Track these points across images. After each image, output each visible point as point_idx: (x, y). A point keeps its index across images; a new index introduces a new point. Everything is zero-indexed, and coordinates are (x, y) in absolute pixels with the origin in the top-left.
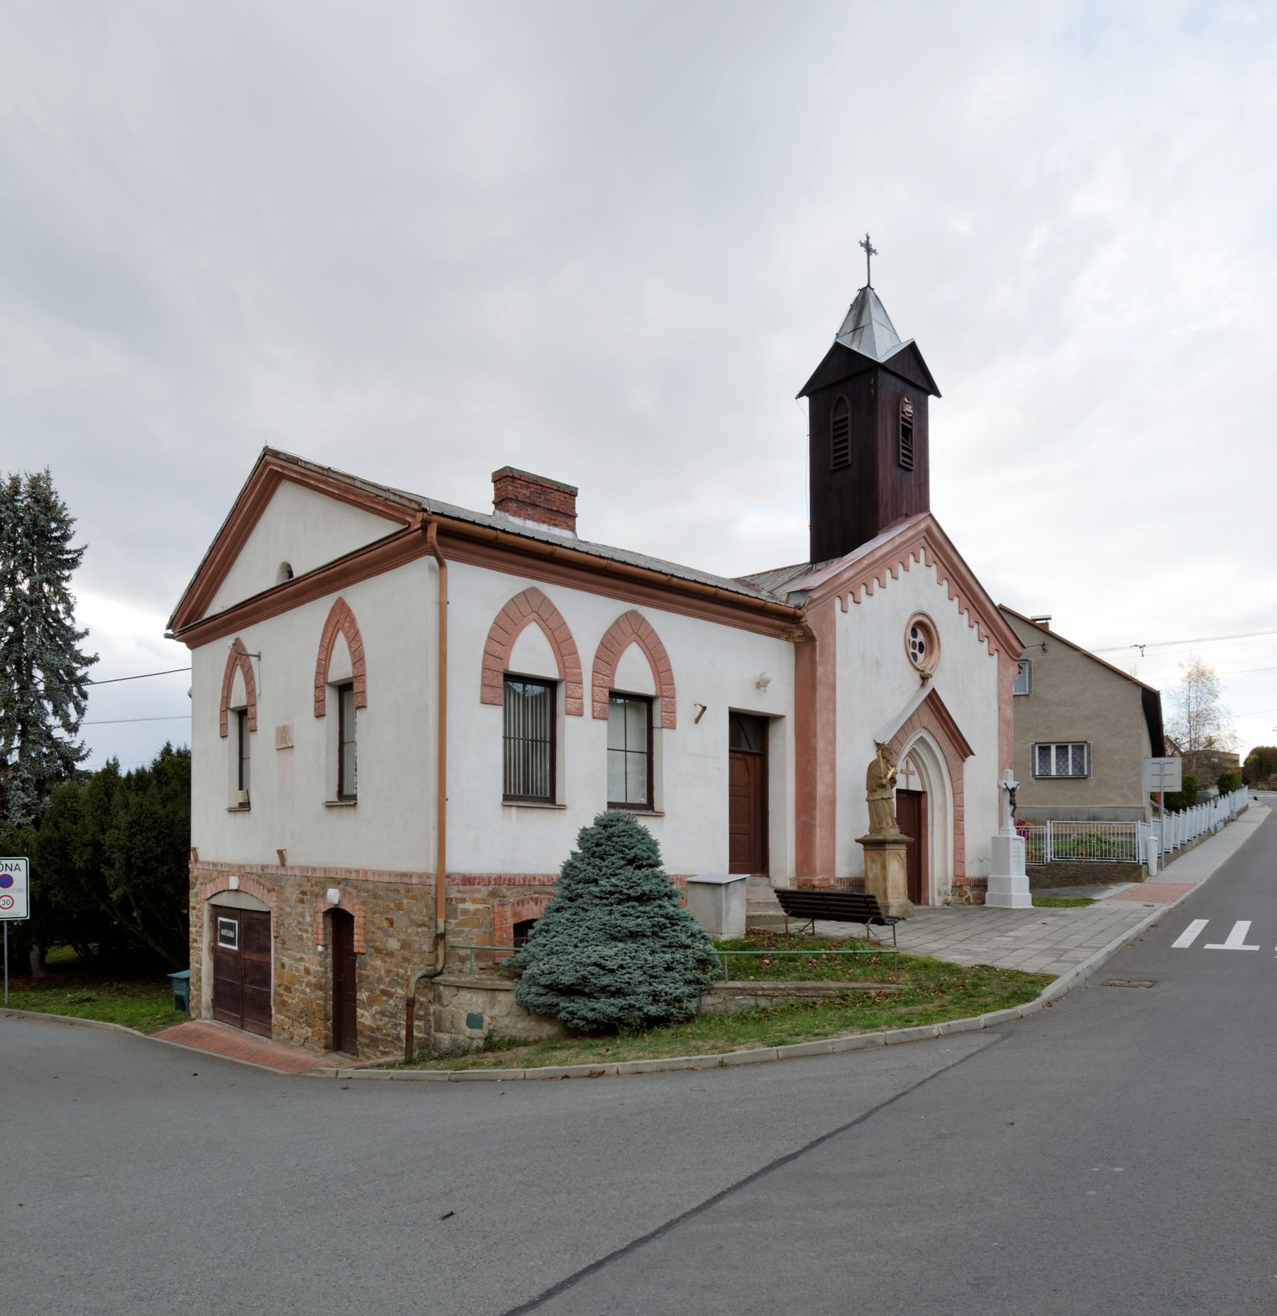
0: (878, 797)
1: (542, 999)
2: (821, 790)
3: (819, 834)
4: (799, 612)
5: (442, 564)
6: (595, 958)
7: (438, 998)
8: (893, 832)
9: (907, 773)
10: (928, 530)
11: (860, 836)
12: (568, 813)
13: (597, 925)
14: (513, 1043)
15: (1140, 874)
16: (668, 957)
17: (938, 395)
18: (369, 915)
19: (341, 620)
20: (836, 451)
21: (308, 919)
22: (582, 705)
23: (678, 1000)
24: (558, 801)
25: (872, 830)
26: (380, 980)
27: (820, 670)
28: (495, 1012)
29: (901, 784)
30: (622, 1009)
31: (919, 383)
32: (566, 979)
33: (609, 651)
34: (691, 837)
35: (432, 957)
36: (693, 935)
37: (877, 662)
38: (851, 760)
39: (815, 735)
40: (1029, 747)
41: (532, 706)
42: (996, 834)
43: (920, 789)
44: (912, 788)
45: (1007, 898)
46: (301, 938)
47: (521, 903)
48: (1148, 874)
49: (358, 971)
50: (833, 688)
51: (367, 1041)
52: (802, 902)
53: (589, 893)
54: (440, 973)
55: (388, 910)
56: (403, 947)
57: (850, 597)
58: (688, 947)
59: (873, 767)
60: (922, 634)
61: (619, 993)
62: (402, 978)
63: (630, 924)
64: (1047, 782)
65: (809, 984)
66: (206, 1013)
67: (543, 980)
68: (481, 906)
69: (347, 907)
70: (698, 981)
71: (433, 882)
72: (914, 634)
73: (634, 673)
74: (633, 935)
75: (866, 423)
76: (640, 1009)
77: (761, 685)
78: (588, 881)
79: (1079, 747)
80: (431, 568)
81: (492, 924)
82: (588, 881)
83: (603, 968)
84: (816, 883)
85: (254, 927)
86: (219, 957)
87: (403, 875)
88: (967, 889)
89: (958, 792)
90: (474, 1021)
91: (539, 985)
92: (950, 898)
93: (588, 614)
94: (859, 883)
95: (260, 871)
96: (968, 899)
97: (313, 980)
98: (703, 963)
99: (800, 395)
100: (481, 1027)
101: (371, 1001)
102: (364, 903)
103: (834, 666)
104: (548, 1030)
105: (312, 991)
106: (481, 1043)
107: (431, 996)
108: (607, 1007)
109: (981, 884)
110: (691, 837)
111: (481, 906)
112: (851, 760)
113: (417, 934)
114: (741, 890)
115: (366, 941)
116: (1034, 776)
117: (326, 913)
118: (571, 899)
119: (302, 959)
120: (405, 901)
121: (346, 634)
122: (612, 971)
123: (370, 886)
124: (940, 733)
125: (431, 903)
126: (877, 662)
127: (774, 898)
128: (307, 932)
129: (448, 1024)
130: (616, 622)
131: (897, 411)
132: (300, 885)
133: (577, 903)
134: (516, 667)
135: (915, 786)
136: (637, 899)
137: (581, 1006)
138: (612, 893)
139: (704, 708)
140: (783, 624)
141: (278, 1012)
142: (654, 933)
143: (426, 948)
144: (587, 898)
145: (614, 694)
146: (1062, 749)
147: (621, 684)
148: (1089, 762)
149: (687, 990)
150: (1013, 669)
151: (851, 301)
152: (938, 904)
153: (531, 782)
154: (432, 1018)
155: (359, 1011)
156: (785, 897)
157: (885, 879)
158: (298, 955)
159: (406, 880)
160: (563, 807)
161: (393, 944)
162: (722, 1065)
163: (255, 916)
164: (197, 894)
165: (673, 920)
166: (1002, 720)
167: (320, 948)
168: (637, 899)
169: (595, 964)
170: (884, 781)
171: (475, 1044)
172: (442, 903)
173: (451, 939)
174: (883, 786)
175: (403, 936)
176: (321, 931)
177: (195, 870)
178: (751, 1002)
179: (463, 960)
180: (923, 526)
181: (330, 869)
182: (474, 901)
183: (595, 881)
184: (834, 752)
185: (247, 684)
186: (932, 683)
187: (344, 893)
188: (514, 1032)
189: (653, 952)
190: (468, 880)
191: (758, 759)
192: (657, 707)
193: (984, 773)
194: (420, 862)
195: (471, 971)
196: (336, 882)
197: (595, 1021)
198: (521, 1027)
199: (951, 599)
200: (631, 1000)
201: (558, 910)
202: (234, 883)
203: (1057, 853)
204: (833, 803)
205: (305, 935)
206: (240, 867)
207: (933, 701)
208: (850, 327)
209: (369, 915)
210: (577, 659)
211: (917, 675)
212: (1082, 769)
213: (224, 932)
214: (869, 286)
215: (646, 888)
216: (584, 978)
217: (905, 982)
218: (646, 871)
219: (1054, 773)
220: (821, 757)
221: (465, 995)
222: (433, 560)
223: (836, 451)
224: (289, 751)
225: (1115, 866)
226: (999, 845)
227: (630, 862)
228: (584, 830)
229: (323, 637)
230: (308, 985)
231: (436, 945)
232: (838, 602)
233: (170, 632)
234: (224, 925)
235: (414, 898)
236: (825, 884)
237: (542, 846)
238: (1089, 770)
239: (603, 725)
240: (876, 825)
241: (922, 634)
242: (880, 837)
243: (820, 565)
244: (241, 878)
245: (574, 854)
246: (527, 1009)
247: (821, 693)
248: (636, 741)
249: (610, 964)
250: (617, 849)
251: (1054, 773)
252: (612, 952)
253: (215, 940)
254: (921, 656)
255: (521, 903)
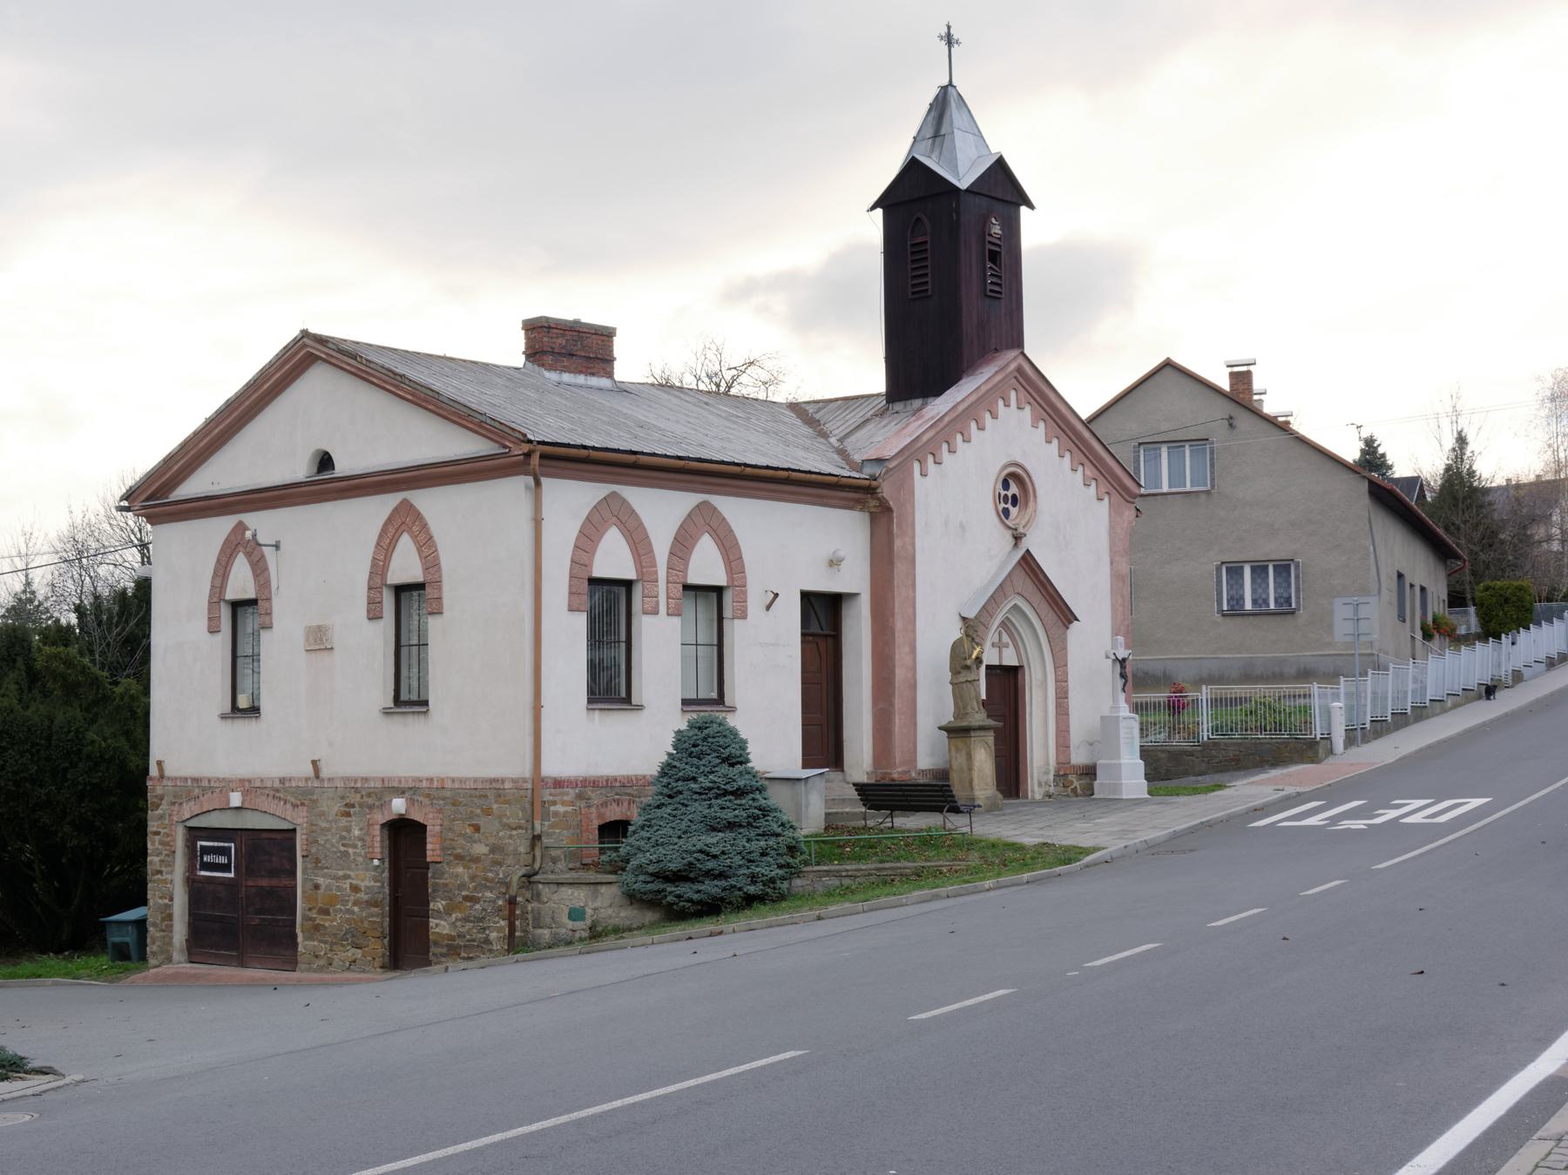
0: (962, 679)
1: (649, 886)
2: (900, 674)
3: (898, 721)
4: (874, 483)
5: (538, 483)
6: (700, 846)
7: (537, 897)
8: (979, 717)
9: (1000, 646)
10: (1019, 370)
11: (944, 723)
12: (645, 712)
13: (698, 818)
14: (617, 931)
15: (1317, 753)
16: (763, 843)
17: (1031, 206)
18: (446, 823)
19: (406, 521)
20: (915, 277)
21: (357, 833)
22: (657, 603)
23: (772, 881)
24: (634, 701)
25: (957, 716)
26: (462, 886)
27: (898, 543)
28: (598, 904)
29: (991, 657)
30: (724, 889)
31: (1009, 198)
32: (673, 866)
33: (682, 545)
34: (770, 733)
35: (530, 857)
36: (783, 825)
37: (962, 526)
38: (933, 635)
39: (893, 615)
40: (1212, 567)
41: (609, 607)
42: (1106, 713)
43: (1016, 663)
44: (1005, 663)
45: (1117, 787)
46: (346, 854)
47: (604, 805)
48: (1331, 752)
49: (431, 881)
50: (912, 561)
51: (444, 950)
52: (884, 795)
53: (690, 790)
54: (536, 873)
55: (472, 815)
56: (492, 851)
57: (930, 459)
58: (778, 835)
59: (956, 647)
60: (1015, 489)
61: (722, 875)
62: (492, 881)
63: (729, 815)
64: (1239, 620)
65: (887, 865)
66: (178, 956)
67: (651, 869)
68: (569, 809)
69: (417, 816)
70: (788, 866)
71: (529, 786)
72: (1006, 485)
73: (706, 566)
74: (731, 826)
75: (950, 261)
76: (740, 889)
77: (834, 563)
78: (686, 779)
79: (1283, 569)
80: (527, 488)
81: (580, 824)
82: (686, 779)
83: (708, 854)
84: (895, 776)
85: (268, 852)
86: (198, 893)
87: (496, 780)
88: (1072, 778)
89: (1061, 664)
90: (576, 914)
91: (647, 873)
92: (1052, 790)
93: (661, 511)
94: (943, 774)
95: (277, 784)
96: (1074, 791)
97: (363, 896)
98: (792, 849)
99: (873, 208)
100: (583, 919)
101: (449, 911)
102: (440, 811)
103: (913, 537)
104: (650, 916)
105: (362, 909)
106: (585, 934)
107: (529, 896)
108: (711, 888)
109: (1090, 772)
110: (770, 733)
111: (569, 809)
112: (933, 635)
113: (511, 837)
114: (820, 784)
115: (443, 849)
116: (1221, 611)
117: (383, 825)
118: (670, 797)
119: (347, 877)
120: (495, 806)
121: (414, 538)
122: (715, 857)
123: (448, 794)
124: (1037, 598)
125: (528, 806)
126: (962, 526)
127: (853, 794)
128: (355, 846)
129: (548, 920)
130: (689, 515)
131: (983, 233)
132: (343, 798)
133: (677, 799)
134: (598, 573)
135: (1010, 659)
136: (732, 793)
137: (686, 889)
138: (710, 789)
139: (776, 595)
140: (856, 496)
141: (308, 938)
142: (749, 824)
143: (522, 850)
144: (686, 794)
145: (687, 588)
146: (1259, 570)
147: (694, 578)
148: (1298, 589)
149: (780, 872)
150: (1129, 513)
151: (931, 99)
152: (1038, 797)
153: (610, 686)
154: (530, 916)
155: (433, 922)
156: (860, 788)
157: (970, 769)
158: (341, 873)
159: (498, 785)
160: (640, 708)
161: (480, 849)
162: (819, 918)
163: (265, 835)
164: (161, 817)
165: (765, 811)
166: (1116, 576)
167: (376, 862)
168: (732, 793)
169: (701, 851)
170: (968, 662)
171: (577, 935)
172: (538, 805)
173: (545, 840)
174: (968, 668)
175: (492, 840)
176: (377, 844)
177: (154, 788)
178: (837, 882)
179: (554, 861)
180: (1013, 366)
181: (390, 779)
182: (563, 803)
183: (694, 779)
184: (914, 631)
185: (256, 576)
186: (1027, 543)
187: (411, 802)
188: (617, 921)
189: (749, 840)
190: (558, 783)
191: (830, 641)
192: (728, 598)
193: (1094, 641)
194: (511, 765)
195: (562, 870)
196: (400, 792)
197: (700, 902)
198: (628, 915)
199: (1048, 442)
200: (732, 881)
201: (658, 807)
202: (236, 799)
203: (1216, 729)
204: (913, 686)
205: (351, 851)
206: (242, 781)
207: (1028, 564)
208: (929, 132)
209: (446, 823)
210: (654, 558)
211: (1008, 535)
212: (1288, 601)
213: (223, 860)
214: (950, 83)
215: (741, 783)
216: (691, 863)
217: (974, 859)
218: (739, 768)
219: (1248, 606)
220: (900, 638)
221: (566, 892)
222: (530, 480)
223: (915, 277)
224: (326, 653)
225: (1286, 743)
226: (1109, 724)
227: (725, 760)
228: (679, 732)
229: (381, 536)
230: (356, 903)
231: (533, 847)
232: (916, 466)
233: (125, 503)
234: (205, 851)
235: (508, 802)
236: (906, 777)
237: (638, 744)
238: (1298, 602)
239: (677, 621)
240: (960, 711)
241: (1015, 489)
242: (965, 724)
243: (898, 406)
244: (245, 793)
245: (670, 754)
246: (632, 898)
247: (900, 567)
248: (707, 634)
249: (714, 851)
250: (708, 748)
251: (1248, 606)
252: (714, 840)
253: (191, 869)
254: (1014, 511)
255: (604, 805)
